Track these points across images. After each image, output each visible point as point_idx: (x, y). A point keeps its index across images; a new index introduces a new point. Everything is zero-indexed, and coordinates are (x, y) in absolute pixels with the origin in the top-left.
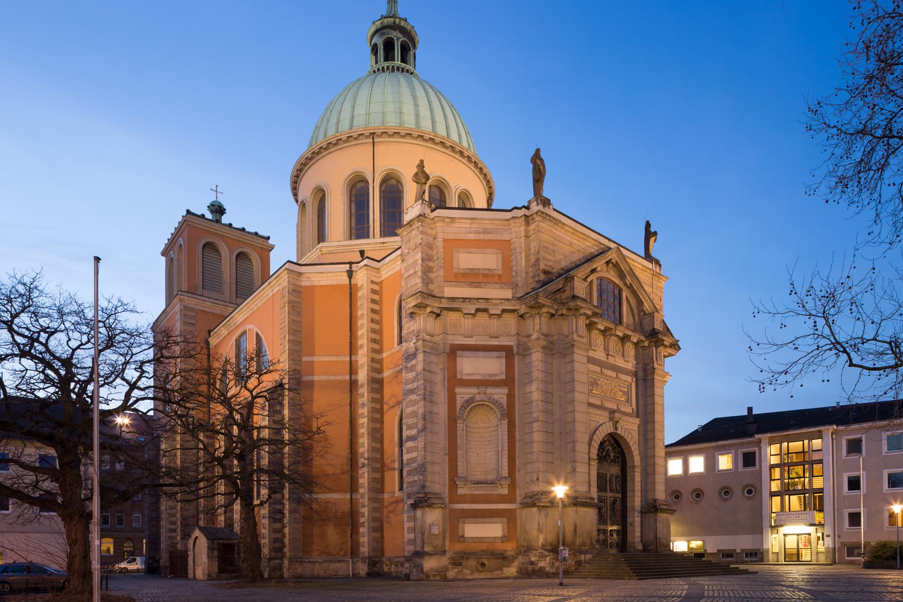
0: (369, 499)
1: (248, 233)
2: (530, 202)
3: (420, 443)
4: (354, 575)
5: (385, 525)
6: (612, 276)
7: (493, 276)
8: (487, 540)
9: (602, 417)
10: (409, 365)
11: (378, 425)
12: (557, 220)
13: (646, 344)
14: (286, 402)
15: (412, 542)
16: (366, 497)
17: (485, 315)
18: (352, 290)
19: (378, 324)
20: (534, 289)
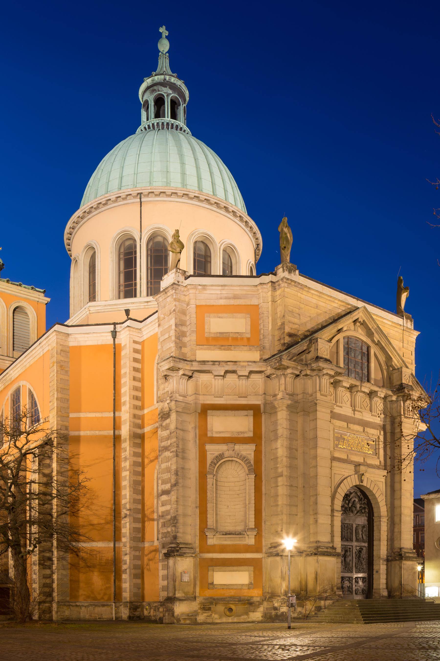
0: (131, 548)
3: (173, 497)
4: (116, 618)
5: (145, 571)
7: (242, 339)
8: (235, 587)
9: (347, 470)
10: (164, 424)
11: (140, 478)
13: (394, 398)
14: (54, 456)
16: (128, 545)
17: (234, 376)
18: (116, 350)
19: (140, 381)
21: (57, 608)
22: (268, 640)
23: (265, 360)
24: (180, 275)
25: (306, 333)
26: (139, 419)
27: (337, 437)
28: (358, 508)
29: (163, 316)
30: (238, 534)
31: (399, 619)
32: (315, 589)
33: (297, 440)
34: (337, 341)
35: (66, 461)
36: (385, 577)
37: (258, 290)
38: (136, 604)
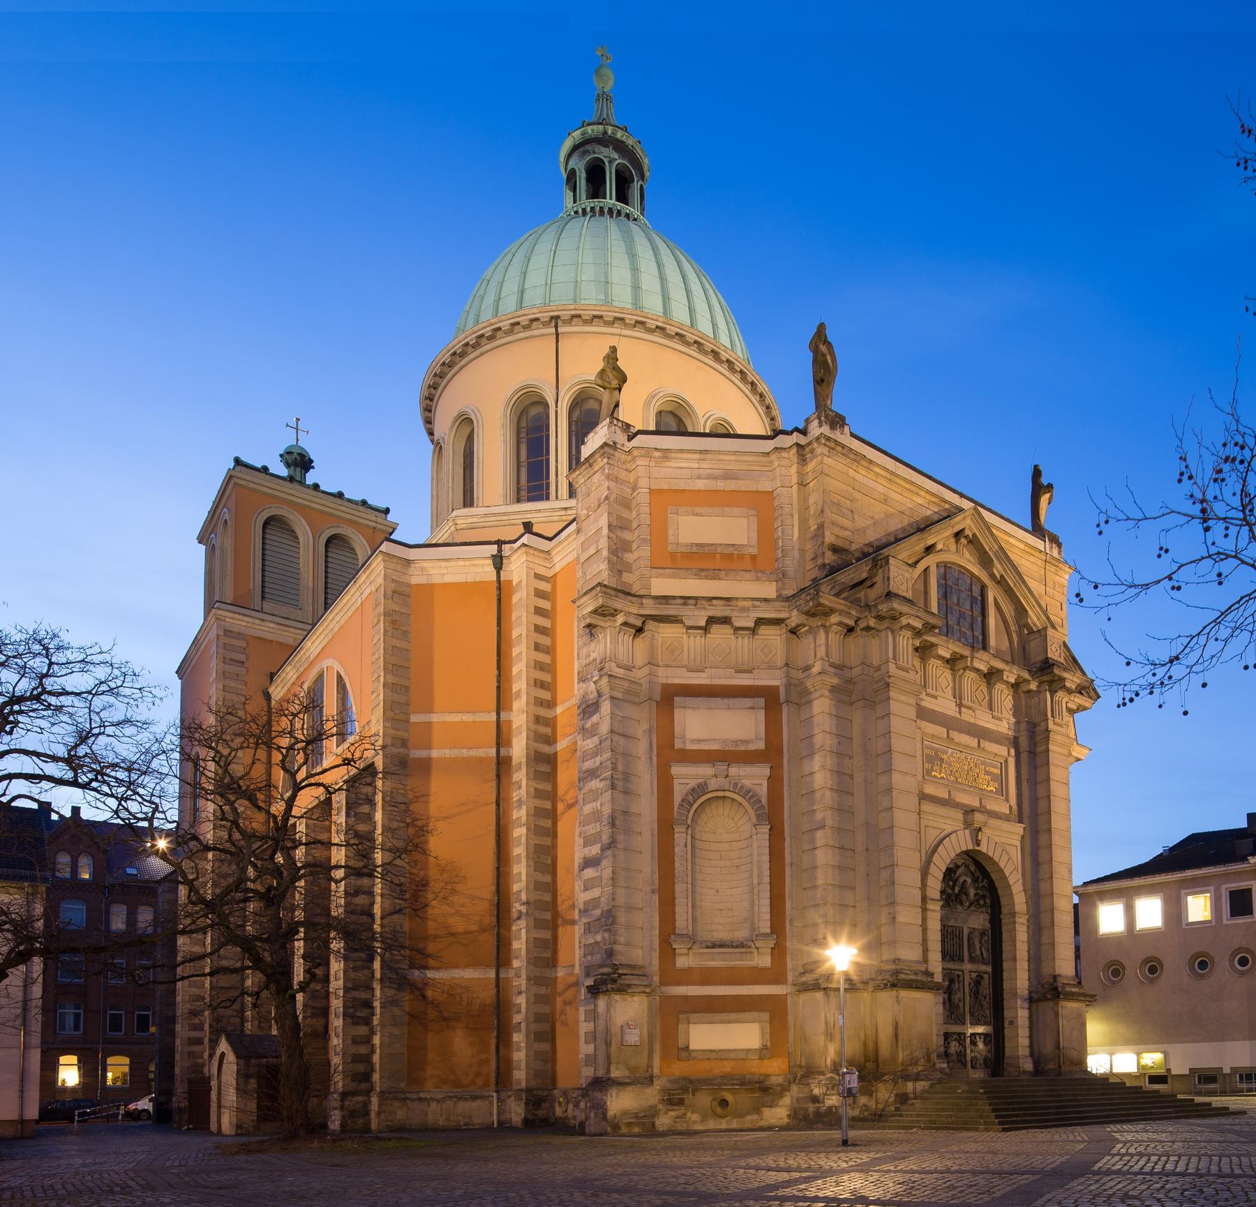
0: (528, 979)
1: (350, 501)
2: (808, 421)
3: (606, 870)
4: (500, 1123)
5: (558, 1026)
6: (967, 560)
7: (741, 557)
8: (733, 1055)
9: (950, 821)
11: (547, 841)
12: (857, 454)
13: (1033, 686)
14: (379, 798)
15: (591, 1060)
16: (524, 976)
17: (727, 630)
18: (502, 591)
19: (548, 653)
20: (815, 580)
21: (379, 1105)
22: (797, 1181)
23: (788, 599)
24: (618, 431)
25: (866, 550)
26: (547, 725)
27: (928, 756)
28: (972, 896)
29: (585, 512)
30: (737, 947)
31: (1068, 1119)
32: (894, 1058)
33: (851, 758)
34: (926, 570)
35: (402, 807)
36: (1027, 1033)
37: (771, 462)
38: (540, 1093)
